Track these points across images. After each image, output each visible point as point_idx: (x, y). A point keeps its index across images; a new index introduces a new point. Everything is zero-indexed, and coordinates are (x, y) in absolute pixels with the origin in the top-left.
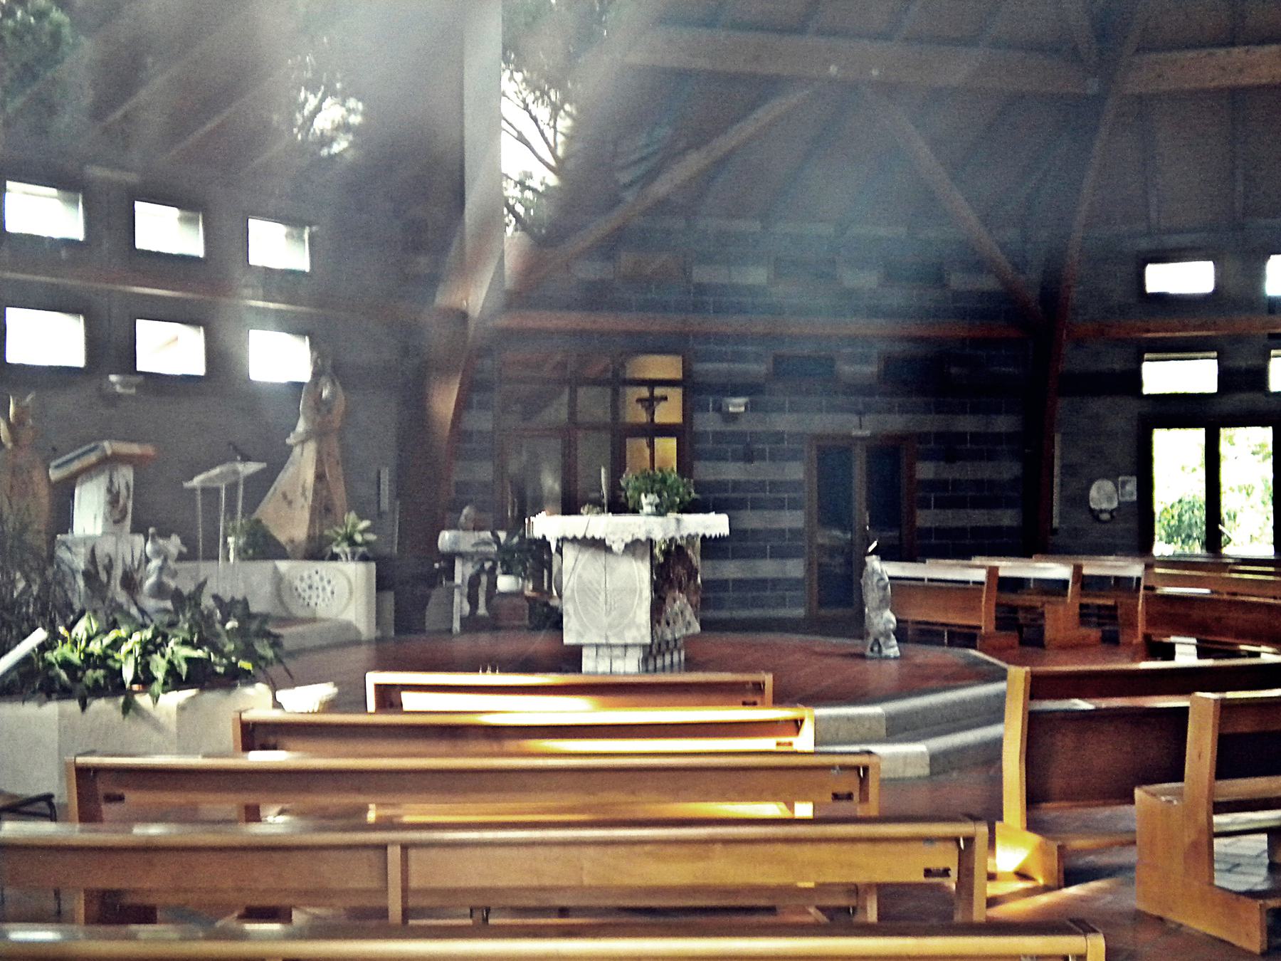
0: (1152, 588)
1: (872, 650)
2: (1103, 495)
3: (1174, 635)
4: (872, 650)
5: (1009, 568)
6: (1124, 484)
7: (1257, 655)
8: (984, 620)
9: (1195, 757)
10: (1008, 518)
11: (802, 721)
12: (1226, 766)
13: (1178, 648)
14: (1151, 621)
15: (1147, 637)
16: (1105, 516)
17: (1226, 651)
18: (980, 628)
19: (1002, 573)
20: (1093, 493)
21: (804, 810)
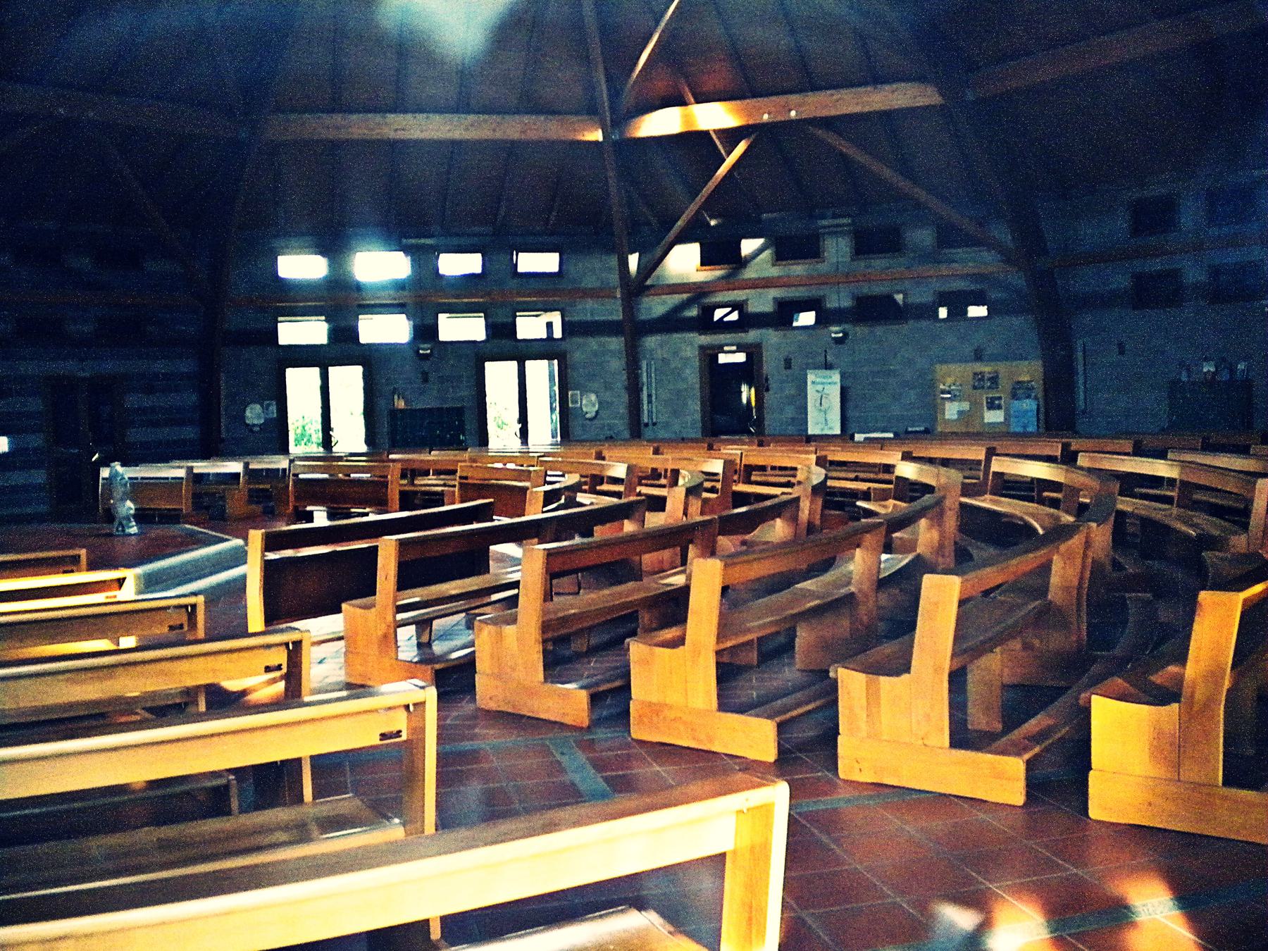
0: (296, 475)
1: (117, 530)
2: (254, 414)
3: (310, 505)
4: (117, 530)
5: (201, 467)
6: (268, 405)
7: (366, 514)
8: (185, 506)
9: (383, 578)
10: (190, 433)
11: (124, 579)
12: (404, 582)
13: (315, 514)
14: (297, 498)
15: (296, 508)
16: (257, 429)
17: (342, 514)
18: (181, 510)
19: (195, 471)
20: (248, 413)
21: (128, 642)
